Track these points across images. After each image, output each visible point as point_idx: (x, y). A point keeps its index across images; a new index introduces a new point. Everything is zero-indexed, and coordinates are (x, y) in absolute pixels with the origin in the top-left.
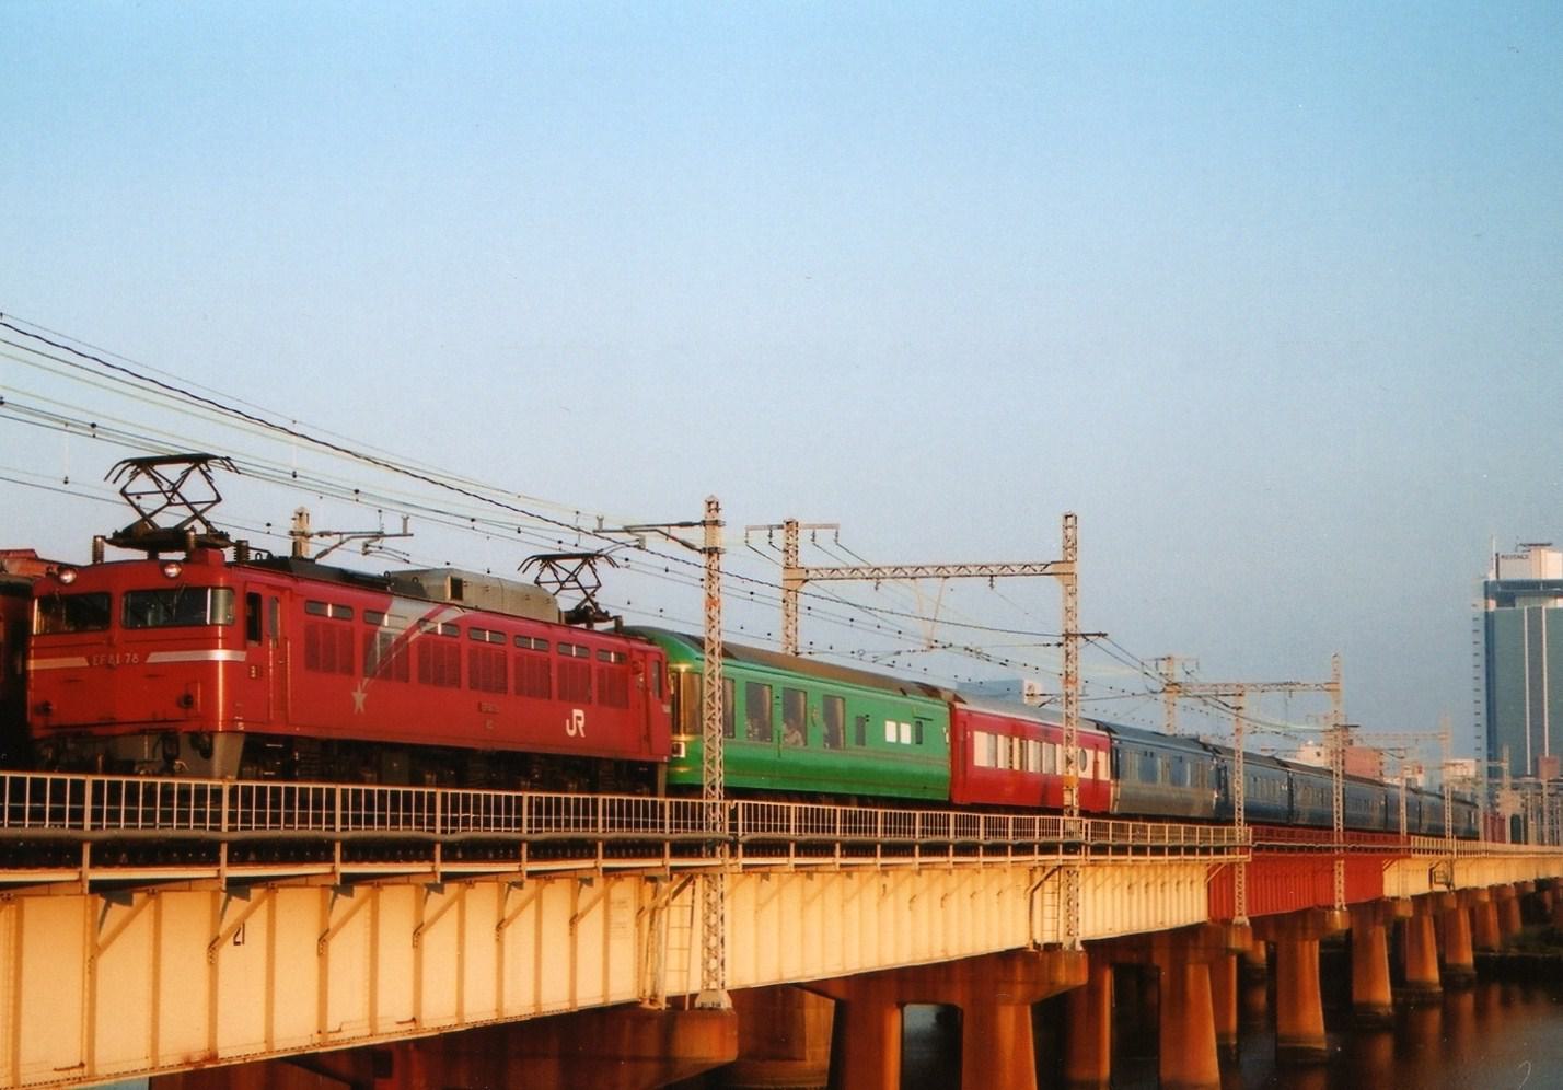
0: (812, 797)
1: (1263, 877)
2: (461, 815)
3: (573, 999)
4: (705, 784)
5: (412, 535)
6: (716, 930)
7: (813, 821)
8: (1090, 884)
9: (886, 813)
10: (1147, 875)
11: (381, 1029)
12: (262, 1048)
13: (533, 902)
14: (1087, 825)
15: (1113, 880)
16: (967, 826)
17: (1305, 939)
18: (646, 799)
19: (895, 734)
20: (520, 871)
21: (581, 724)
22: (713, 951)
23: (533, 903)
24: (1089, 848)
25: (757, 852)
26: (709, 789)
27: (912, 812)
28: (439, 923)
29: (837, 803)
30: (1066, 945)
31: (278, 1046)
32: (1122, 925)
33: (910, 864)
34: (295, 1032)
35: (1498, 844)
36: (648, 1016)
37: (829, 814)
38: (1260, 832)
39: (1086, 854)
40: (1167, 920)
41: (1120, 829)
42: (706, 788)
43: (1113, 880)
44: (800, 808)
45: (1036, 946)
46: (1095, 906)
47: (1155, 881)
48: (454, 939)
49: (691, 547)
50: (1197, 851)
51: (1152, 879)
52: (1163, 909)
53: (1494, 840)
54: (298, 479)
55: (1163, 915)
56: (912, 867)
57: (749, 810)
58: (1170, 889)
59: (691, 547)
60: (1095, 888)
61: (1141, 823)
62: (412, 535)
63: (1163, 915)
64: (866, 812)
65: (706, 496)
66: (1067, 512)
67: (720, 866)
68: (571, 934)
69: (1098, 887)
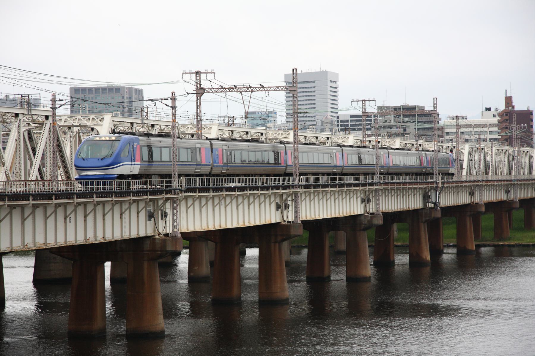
0: (252, 175)
2: (120, 186)
4: (172, 173)
9: (199, 179)
11: (58, 244)
13: (264, 202)
16: (341, 179)
17: (275, 242)
19: (188, 151)
20: (131, 200)
22: (297, 212)
24: (303, 187)
25: (153, 194)
26: (174, 175)
28: (50, 217)
29: (352, 175)
30: (515, 200)
31: (132, 236)
33: (269, 193)
34: (80, 240)
37: (194, 180)
38: (325, 179)
39: (302, 189)
40: (410, 207)
41: (341, 179)
44: (213, 179)
45: (473, 203)
47: (451, 191)
49: (168, 106)
52: (414, 204)
54: (74, 108)
55: (449, 203)
57: (199, 180)
59: (168, 106)
61: (350, 176)
63: (449, 203)
64: (219, 179)
65: (172, 91)
66: (293, 68)
69: (392, 196)
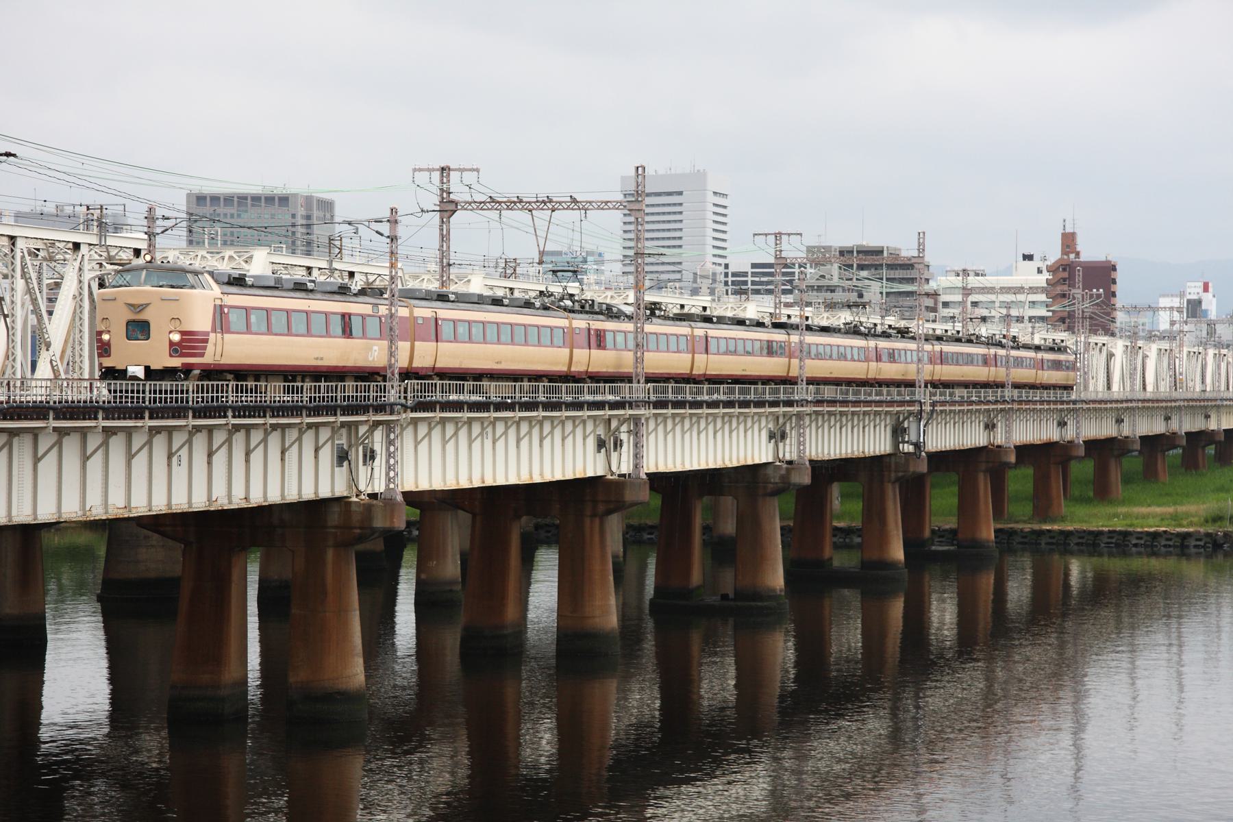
1: (969, 421)
5: (921, 236)
8: (935, 422)
12: (297, 497)
14: (649, 390)
15: (886, 422)
21: (376, 354)
23: (262, 445)
32: (880, 450)
40: (866, 451)
43: (683, 426)
46: (760, 441)
47: (869, 423)
49: (382, 235)
50: (147, 415)
51: (973, 419)
56: (605, 417)
59: (382, 235)
62: (921, 236)
67: (185, 426)
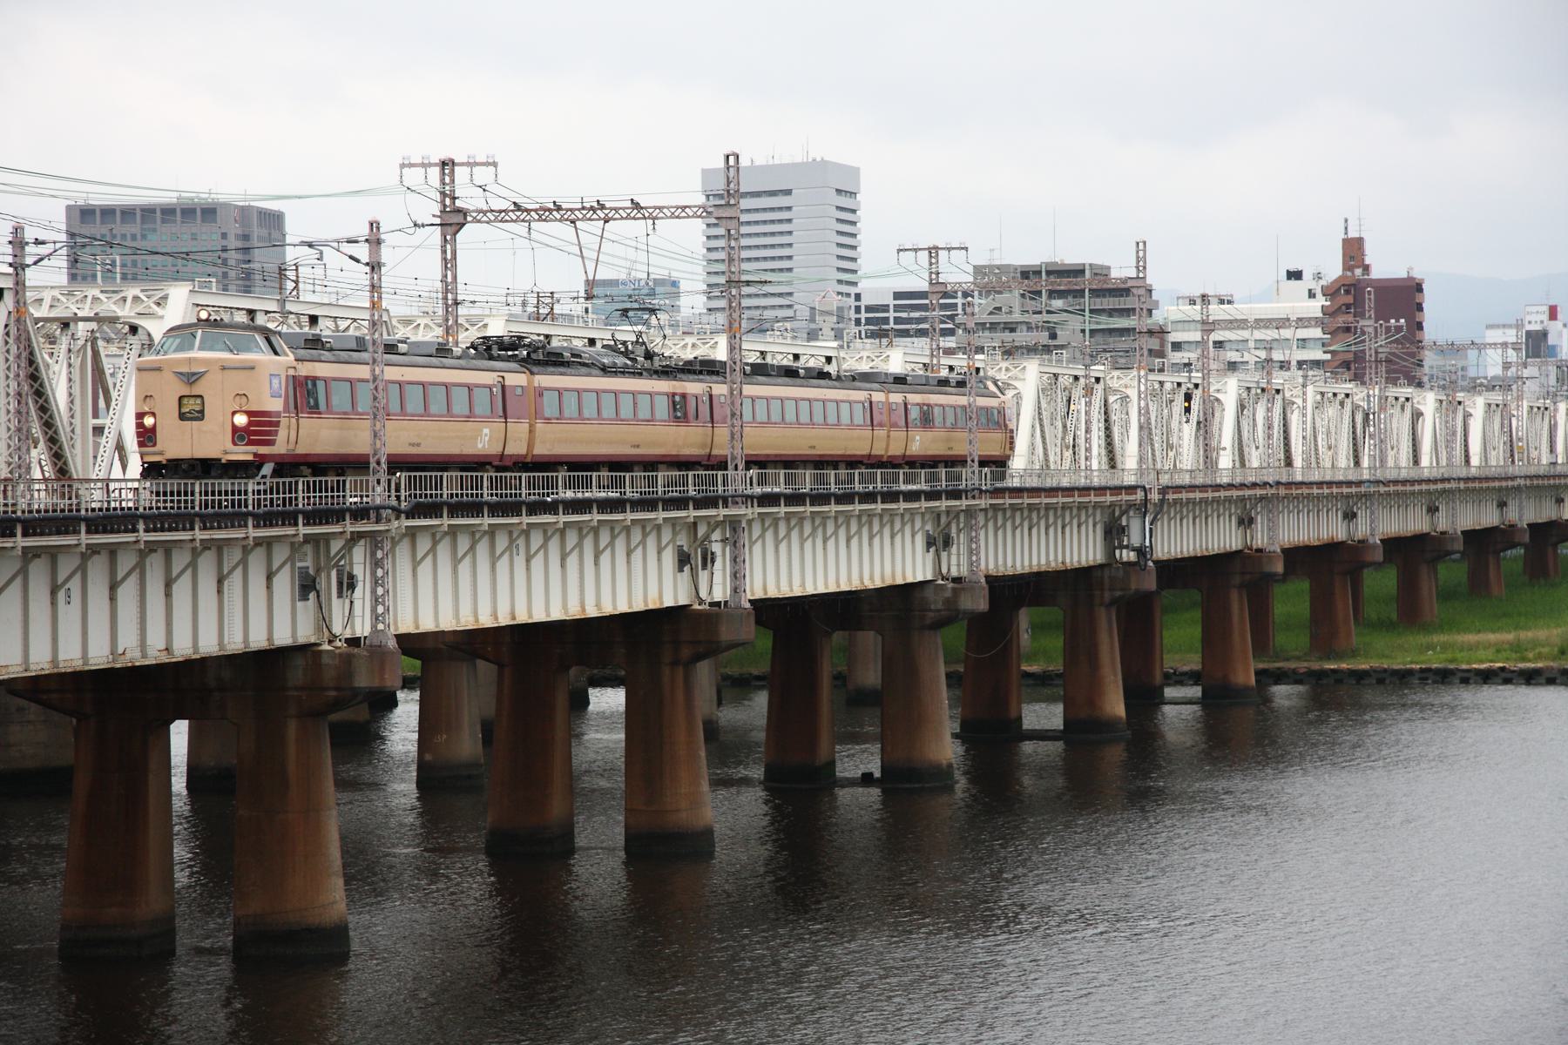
3: (270, 639)
6: (383, 582)
7: (820, 480)
10: (1079, 516)
13: (289, 564)
16: (932, 478)
17: (675, 663)
18: (700, 473)
24: (755, 500)
26: (375, 465)
27: (622, 474)
30: (1371, 541)
35: (679, 391)
36: (1249, 557)
40: (1068, 560)
42: (373, 465)
48: (190, 592)
49: (358, 261)
51: (1221, 511)
53: (684, 396)
58: (1211, 521)
59: (358, 261)
60: (1014, 528)
68: (52, 603)
